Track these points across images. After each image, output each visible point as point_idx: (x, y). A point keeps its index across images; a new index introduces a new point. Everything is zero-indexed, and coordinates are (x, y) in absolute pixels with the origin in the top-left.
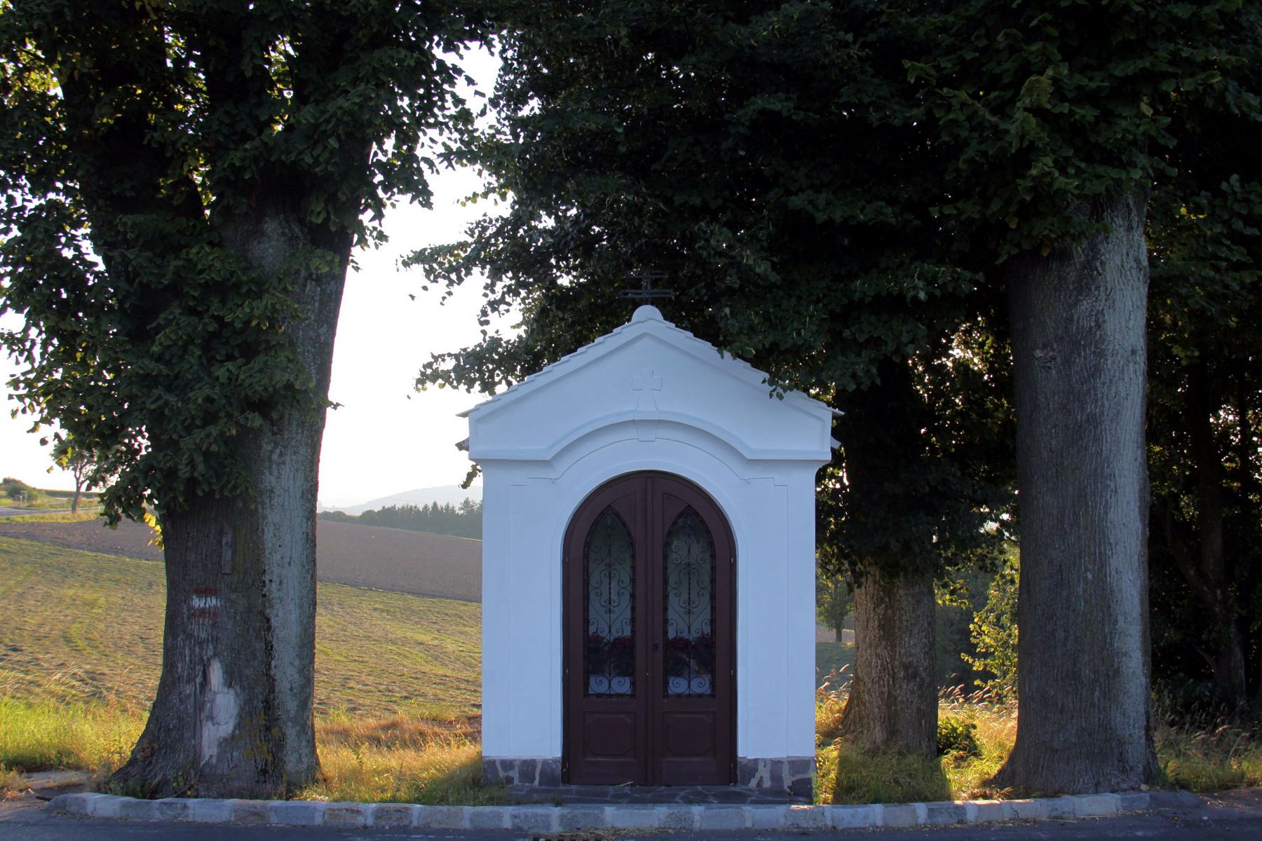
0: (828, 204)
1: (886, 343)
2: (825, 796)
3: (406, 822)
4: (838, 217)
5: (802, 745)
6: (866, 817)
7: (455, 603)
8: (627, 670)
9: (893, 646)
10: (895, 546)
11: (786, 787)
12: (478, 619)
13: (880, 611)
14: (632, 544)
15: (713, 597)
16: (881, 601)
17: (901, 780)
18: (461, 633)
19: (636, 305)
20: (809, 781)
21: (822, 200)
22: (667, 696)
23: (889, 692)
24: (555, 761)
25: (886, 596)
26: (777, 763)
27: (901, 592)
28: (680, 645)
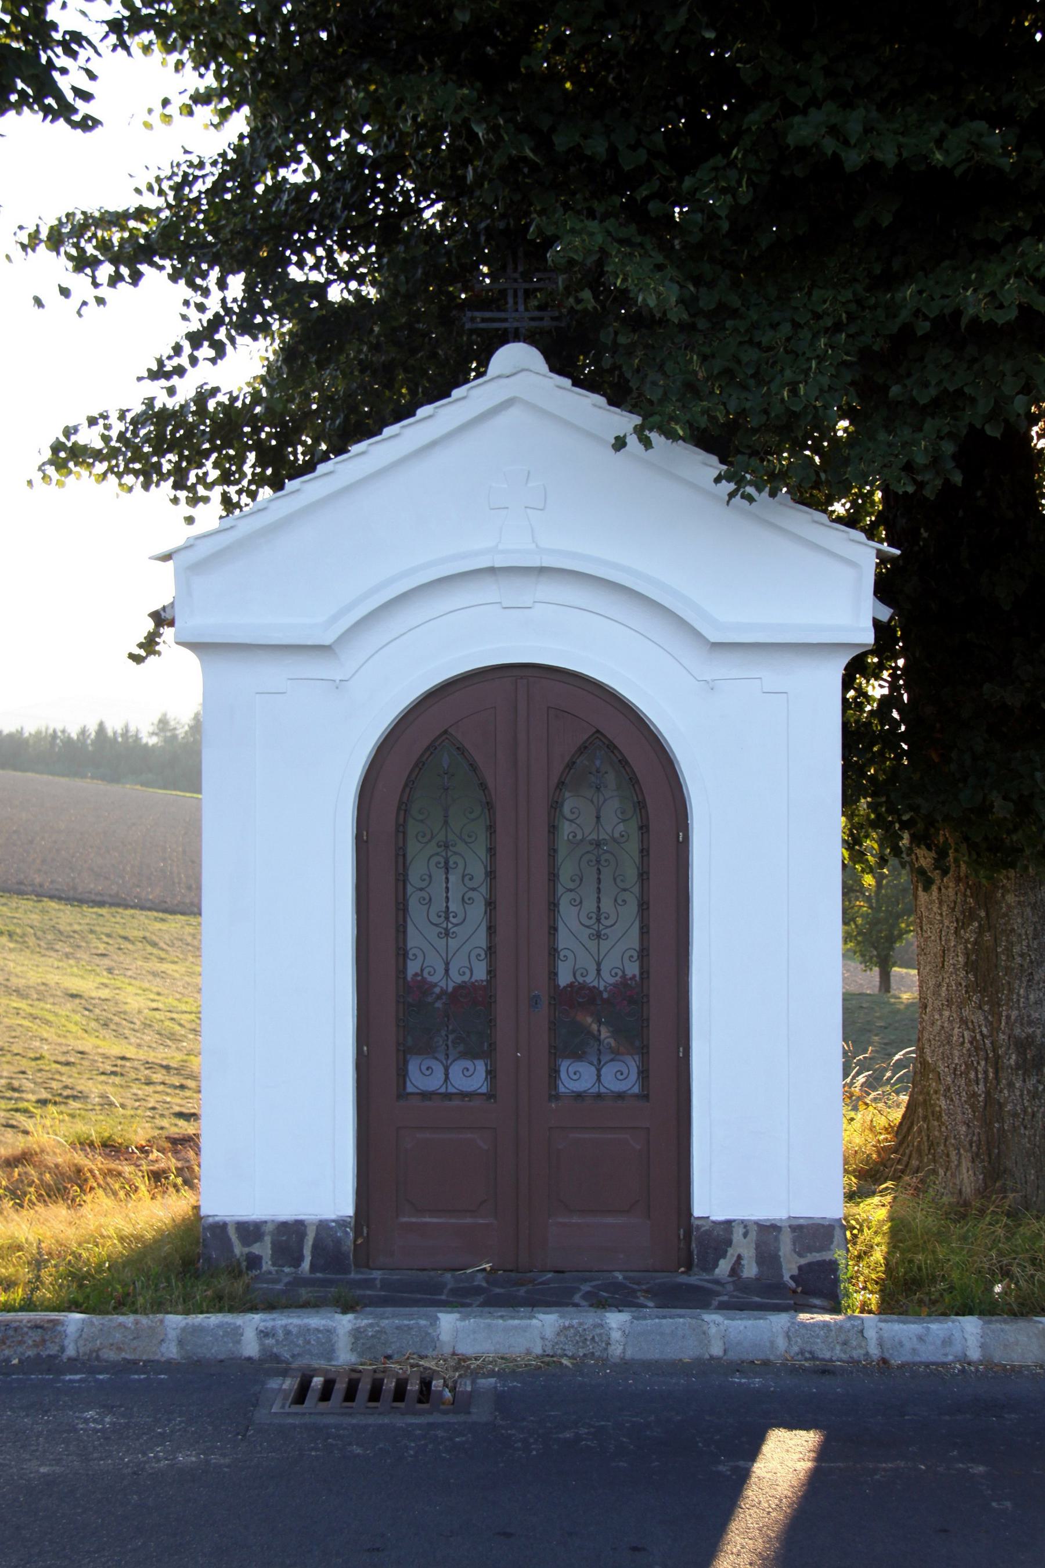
0: (868, 130)
1: (973, 400)
2: (862, 1296)
3: (53, 1350)
4: (888, 156)
5: (821, 1197)
6: (947, 1342)
7: (142, 916)
8: (478, 1045)
9: (995, 1004)
10: (1001, 809)
11: (786, 1278)
12: (193, 948)
13: (969, 934)
14: (489, 806)
15: (644, 906)
16: (970, 915)
17: (1016, 1270)
18: (155, 974)
19: (504, 338)
20: (832, 1266)
21: (854, 123)
22: (557, 1097)
23: (988, 1093)
24: (341, 1223)
25: (979, 908)
26: (768, 1230)
27: (1011, 898)
28: (581, 997)
